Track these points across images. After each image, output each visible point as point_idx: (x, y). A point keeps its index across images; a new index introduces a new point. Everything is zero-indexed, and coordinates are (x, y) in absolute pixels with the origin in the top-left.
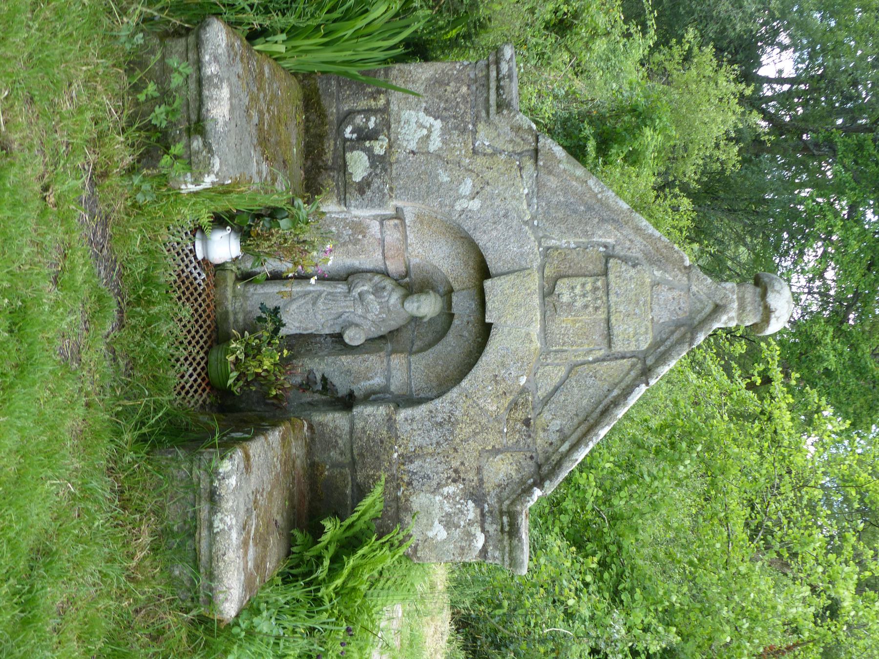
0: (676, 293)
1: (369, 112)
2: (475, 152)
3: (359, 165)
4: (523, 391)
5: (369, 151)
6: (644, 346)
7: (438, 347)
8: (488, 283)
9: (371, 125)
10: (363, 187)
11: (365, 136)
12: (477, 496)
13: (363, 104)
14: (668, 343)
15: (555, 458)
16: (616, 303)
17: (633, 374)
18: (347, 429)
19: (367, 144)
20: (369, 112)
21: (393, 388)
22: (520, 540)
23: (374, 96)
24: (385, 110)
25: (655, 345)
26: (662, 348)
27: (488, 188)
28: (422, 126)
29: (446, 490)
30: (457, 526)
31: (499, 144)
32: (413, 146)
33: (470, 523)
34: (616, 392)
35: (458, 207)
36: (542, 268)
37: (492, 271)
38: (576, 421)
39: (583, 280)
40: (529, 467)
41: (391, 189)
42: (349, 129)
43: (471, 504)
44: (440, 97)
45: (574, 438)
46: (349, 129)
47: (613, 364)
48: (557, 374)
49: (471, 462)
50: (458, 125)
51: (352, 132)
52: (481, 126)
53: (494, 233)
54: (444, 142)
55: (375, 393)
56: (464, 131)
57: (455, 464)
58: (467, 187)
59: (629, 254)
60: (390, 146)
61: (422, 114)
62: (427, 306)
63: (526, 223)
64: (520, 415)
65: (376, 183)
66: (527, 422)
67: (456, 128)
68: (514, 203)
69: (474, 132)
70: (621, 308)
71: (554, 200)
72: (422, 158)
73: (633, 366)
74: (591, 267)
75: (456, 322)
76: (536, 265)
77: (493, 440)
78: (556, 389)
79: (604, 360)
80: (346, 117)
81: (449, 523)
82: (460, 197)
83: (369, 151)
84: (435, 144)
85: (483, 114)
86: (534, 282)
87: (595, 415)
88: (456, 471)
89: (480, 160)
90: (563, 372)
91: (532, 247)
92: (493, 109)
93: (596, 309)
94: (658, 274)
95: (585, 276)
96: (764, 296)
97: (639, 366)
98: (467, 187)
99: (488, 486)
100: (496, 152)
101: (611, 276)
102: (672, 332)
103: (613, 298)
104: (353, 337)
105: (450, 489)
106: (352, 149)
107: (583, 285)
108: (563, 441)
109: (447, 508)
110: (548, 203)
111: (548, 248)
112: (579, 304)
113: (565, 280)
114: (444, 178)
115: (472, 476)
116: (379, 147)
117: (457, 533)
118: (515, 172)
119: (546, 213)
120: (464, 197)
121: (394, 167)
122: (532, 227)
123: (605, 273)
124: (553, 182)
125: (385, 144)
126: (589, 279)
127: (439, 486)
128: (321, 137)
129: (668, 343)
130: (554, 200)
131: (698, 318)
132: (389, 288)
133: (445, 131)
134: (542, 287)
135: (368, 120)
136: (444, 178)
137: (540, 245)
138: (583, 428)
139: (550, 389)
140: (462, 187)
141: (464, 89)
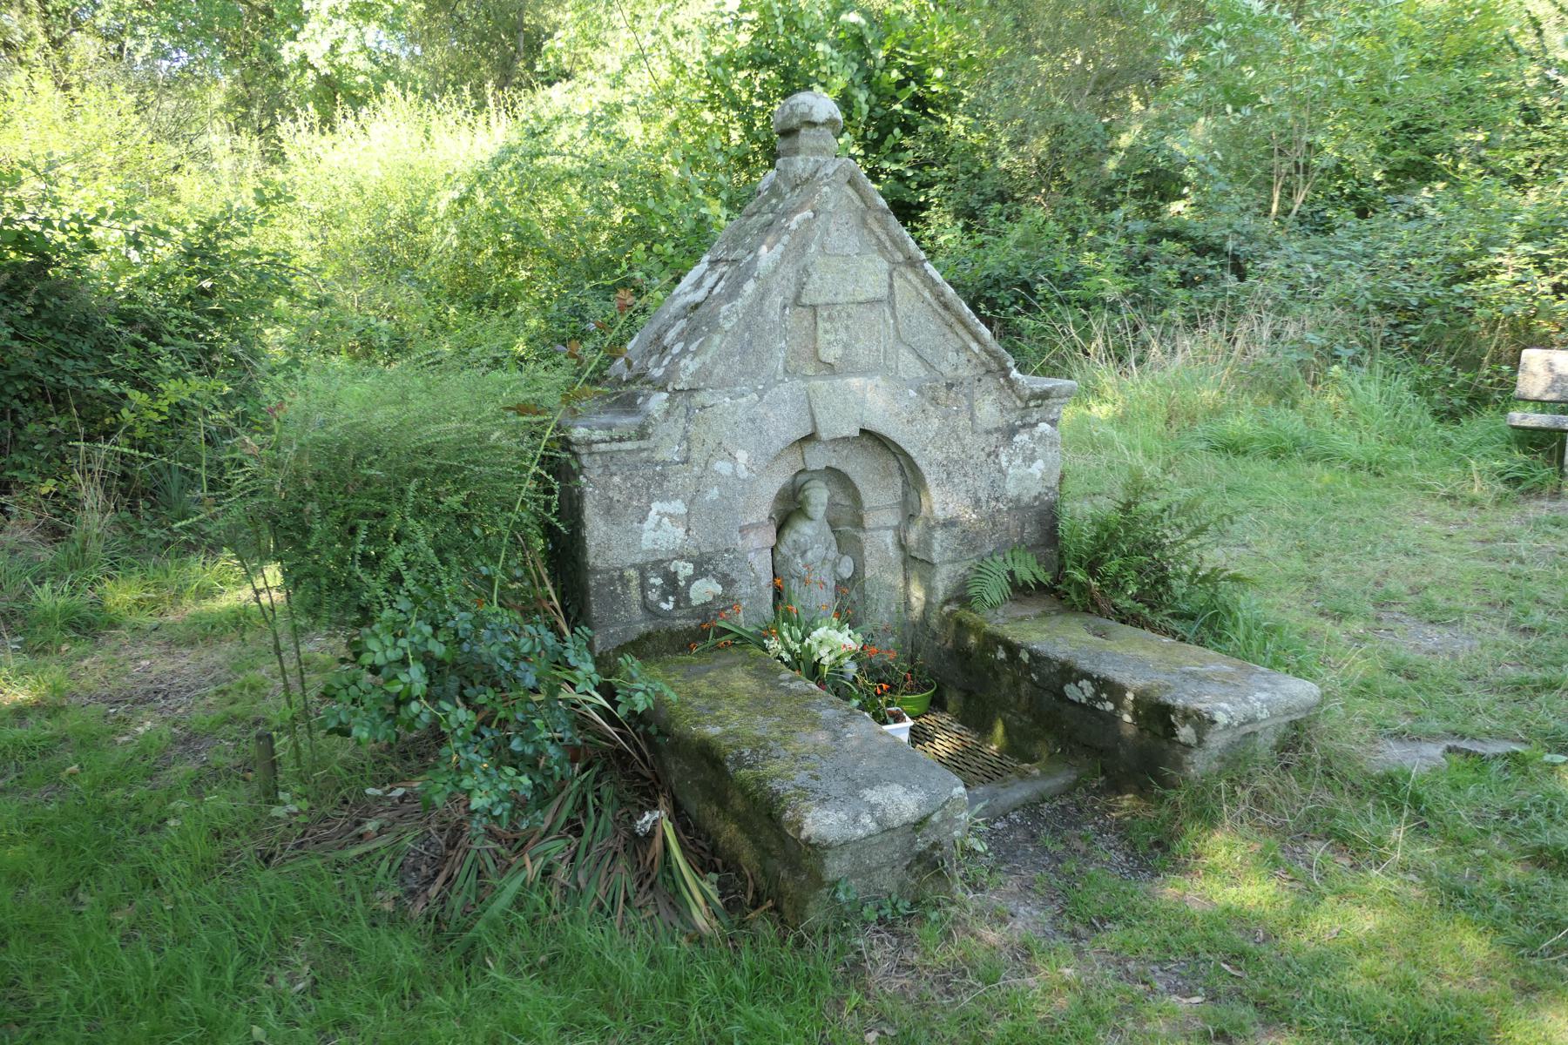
0: (832, 227)
1: (644, 587)
2: (686, 461)
3: (704, 590)
4: (919, 391)
5: (690, 580)
6: (886, 265)
7: (858, 481)
8: (824, 436)
9: (658, 581)
10: (727, 581)
11: (671, 584)
12: (1011, 432)
13: (635, 594)
14: (883, 237)
15: (984, 356)
16: (846, 294)
17: (911, 276)
18: (949, 566)
19: (682, 584)
20: (644, 587)
21: (896, 523)
22: (1053, 389)
23: (625, 582)
24: (642, 570)
25: (882, 249)
26: (888, 244)
27: (725, 442)
28: (659, 524)
29: (1004, 464)
30: (1034, 450)
31: (678, 434)
32: (681, 531)
33: (1032, 437)
34: (927, 294)
35: (746, 474)
36: (805, 378)
37: (809, 431)
38: (950, 336)
39: (820, 332)
40: (989, 382)
41: (727, 551)
42: (664, 606)
43: (1017, 438)
44: (626, 507)
45: (968, 338)
46: (664, 606)
47: (898, 298)
48: (906, 357)
49: (981, 441)
50: (656, 480)
51: (667, 601)
52: (658, 457)
53: (772, 432)
54: (676, 496)
55: (900, 540)
56: (663, 476)
57: (983, 456)
58: (723, 467)
59: (793, 280)
60: (682, 557)
61: (646, 526)
62: (819, 496)
63: (761, 397)
64: (942, 394)
65: (723, 567)
66: (950, 386)
67: (661, 485)
68: (740, 411)
69: (664, 463)
70: (850, 289)
71: (738, 367)
72: (693, 520)
73: (901, 275)
74: (806, 323)
75: (833, 464)
76: (803, 385)
77: (963, 421)
78: (920, 357)
79: (893, 308)
80: (649, 609)
81: (1030, 459)
82: (735, 475)
83: (690, 580)
84: (678, 507)
85: (644, 455)
86: (822, 385)
87: (947, 316)
88: (989, 455)
89: (695, 455)
90: (903, 351)
91: (785, 390)
92: (643, 444)
93: (849, 316)
94: (813, 248)
95: (815, 328)
96: (813, 124)
97: (903, 269)
98: (723, 467)
99: (1001, 423)
100: (686, 437)
101: (820, 300)
102: (872, 232)
103: (840, 298)
104: (846, 570)
105: (1003, 459)
106: (688, 599)
107: (826, 332)
108: (968, 348)
109: (1019, 461)
110: (741, 374)
111: (786, 371)
112: (843, 336)
113: (821, 352)
114: (714, 493)
115: (993, 439)
116: (685, 569)
117: (1039, 450)
118: (708, 414)
119: (753, 375)
120: (734, 468)
121: (703, 550)
122: (764, 391)
123: (814, 307)
124: (720, 370)
125: (681, 564)
126: (821, 324)
127: (1000, 471)
128: (672, 634)
129: (883, 237)
130: (738, 367)
131: (858, 202)
132: (795, 536)
133: (664, 498)
134: (824, 377)
135: (654, 586)
136: (714, 493)
137: (782, 381)
138: (959, 328)
139: (919, 363)
140: (723, 472)
141: (616, 479)
